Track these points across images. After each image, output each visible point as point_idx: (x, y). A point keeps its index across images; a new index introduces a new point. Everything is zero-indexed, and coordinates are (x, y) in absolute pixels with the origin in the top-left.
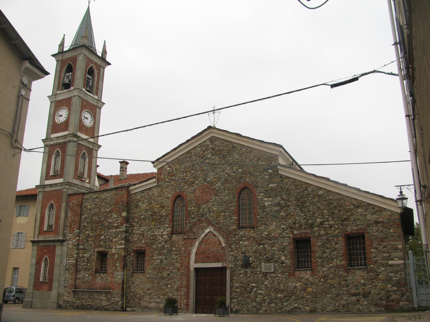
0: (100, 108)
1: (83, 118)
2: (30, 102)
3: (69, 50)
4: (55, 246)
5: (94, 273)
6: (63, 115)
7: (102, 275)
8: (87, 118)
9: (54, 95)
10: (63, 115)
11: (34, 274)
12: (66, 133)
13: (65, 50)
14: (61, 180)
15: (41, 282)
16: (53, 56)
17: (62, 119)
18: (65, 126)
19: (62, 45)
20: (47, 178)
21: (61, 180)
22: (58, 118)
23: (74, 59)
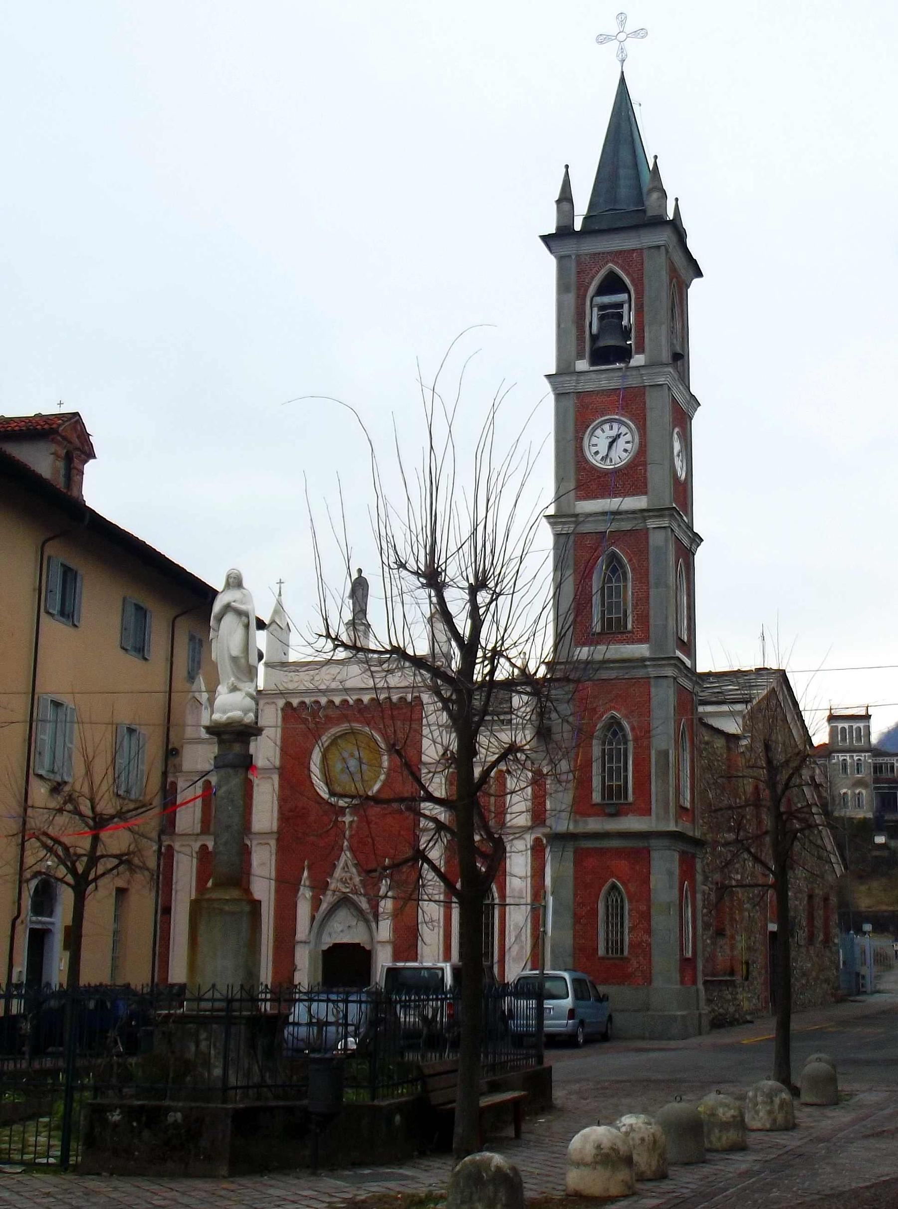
14: (642, 650)
15: (603, 958)
18: (630, 478)
19: (565, 198)
20: (592, 640)
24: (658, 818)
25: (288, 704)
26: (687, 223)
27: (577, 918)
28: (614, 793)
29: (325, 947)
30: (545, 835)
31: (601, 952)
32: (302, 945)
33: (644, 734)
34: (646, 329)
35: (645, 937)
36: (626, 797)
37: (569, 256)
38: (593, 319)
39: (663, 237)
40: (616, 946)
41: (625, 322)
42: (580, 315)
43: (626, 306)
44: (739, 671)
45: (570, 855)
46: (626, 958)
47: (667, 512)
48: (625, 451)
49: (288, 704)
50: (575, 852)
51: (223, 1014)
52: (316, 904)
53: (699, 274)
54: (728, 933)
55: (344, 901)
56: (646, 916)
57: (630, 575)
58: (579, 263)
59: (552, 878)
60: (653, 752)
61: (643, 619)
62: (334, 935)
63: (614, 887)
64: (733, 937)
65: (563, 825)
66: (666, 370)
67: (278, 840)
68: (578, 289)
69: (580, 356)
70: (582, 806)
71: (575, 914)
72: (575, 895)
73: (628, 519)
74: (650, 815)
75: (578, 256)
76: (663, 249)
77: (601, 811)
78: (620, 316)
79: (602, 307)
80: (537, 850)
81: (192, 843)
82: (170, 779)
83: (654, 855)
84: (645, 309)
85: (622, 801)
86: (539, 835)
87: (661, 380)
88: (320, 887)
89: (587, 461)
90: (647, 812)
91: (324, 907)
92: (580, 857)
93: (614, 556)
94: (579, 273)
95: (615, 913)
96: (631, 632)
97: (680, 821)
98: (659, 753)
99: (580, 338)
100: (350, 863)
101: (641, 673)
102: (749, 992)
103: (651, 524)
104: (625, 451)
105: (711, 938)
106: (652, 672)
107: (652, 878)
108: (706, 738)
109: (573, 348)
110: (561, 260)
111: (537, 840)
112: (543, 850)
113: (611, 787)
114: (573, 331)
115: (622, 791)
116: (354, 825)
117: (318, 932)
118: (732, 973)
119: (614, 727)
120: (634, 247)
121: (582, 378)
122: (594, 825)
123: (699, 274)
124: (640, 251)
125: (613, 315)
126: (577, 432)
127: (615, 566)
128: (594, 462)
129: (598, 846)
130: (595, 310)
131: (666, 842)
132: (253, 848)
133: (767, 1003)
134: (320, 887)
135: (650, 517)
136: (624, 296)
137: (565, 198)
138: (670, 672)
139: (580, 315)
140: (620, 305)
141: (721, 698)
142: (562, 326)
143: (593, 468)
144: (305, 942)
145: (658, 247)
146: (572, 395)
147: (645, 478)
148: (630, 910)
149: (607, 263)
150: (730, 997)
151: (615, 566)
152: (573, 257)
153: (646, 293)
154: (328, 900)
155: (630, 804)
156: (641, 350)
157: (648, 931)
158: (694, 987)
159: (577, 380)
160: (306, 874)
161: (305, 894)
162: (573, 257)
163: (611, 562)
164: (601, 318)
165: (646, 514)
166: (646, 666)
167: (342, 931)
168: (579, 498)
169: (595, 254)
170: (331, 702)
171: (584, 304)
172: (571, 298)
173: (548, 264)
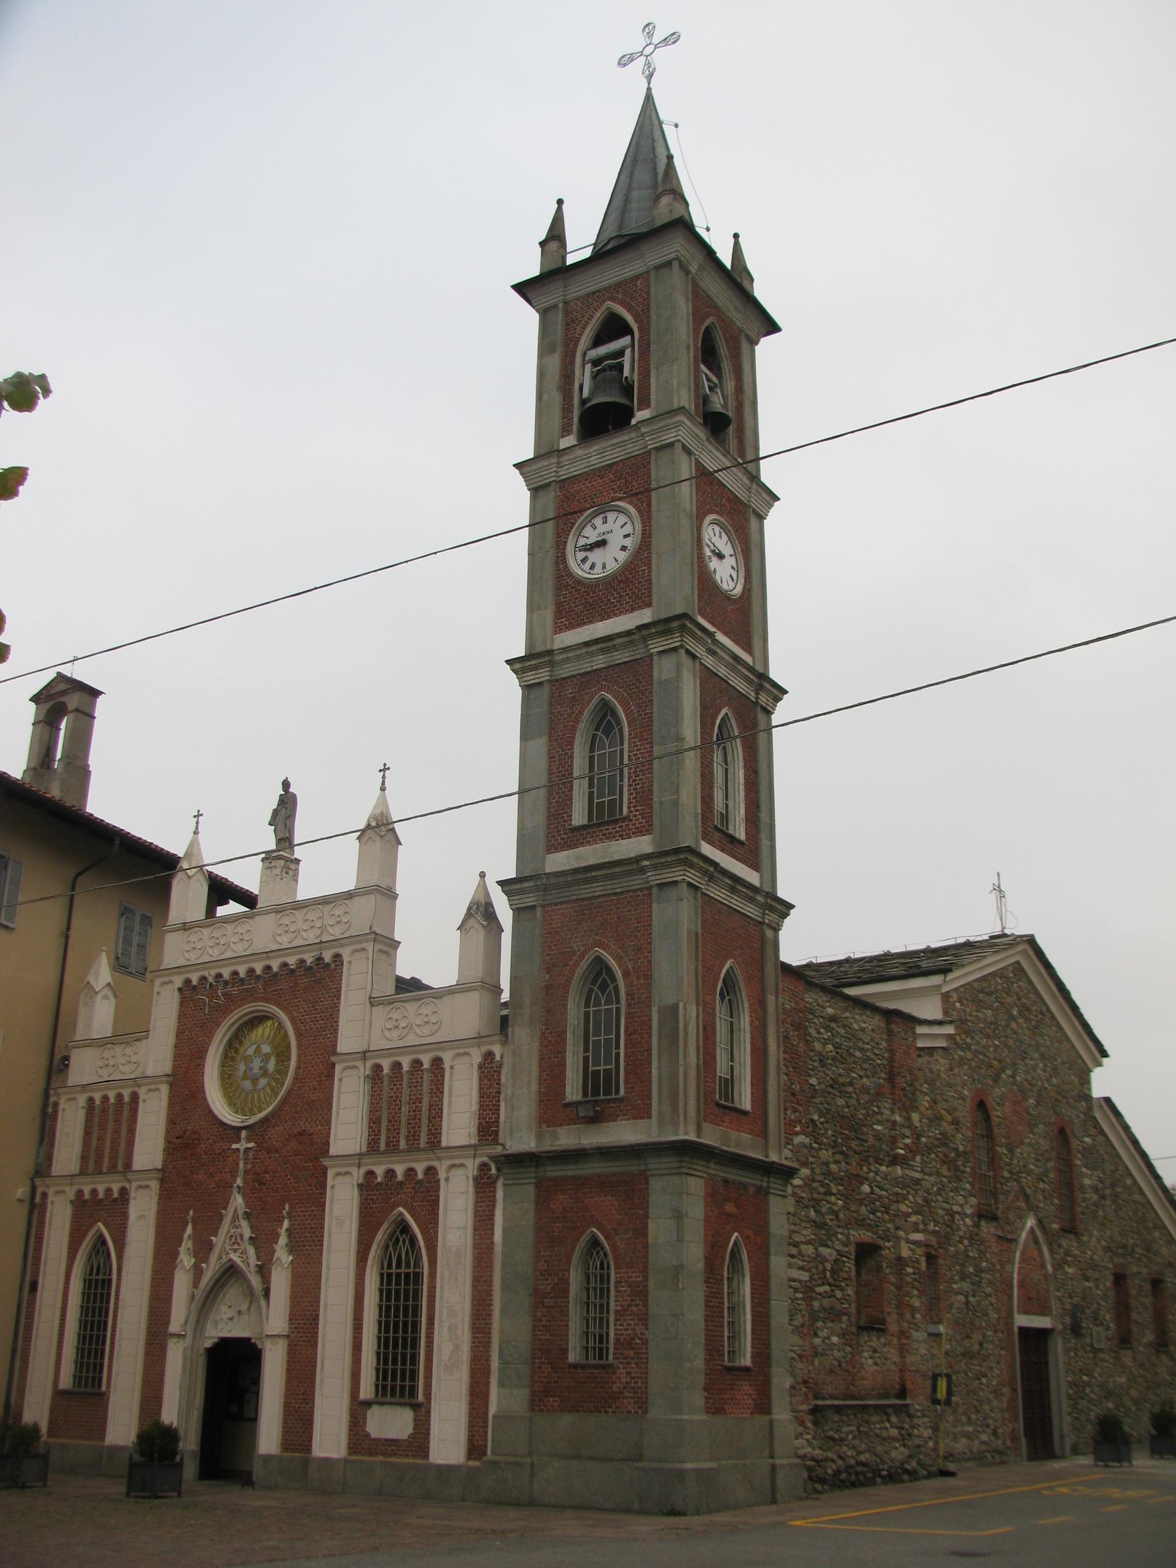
0: (761, 518)
1: (708, 553)
2: (97, 723)
3: (602, 254)
4: (644, 1177)
5: (854, 1329)
6: (608, 542)
7: (874, 1342)
8: (720, 556)
9: (545, 451)
10: (608, 542)
11: (703, 1324)
12: (645, 616)
13: (571, 260)
14: (642, 845)
15: (575, 1366)
16: (522, 288)
17: (610, 560)
18: (631, 584)
19: (556, 235)
20: (572, 837)
21: (642, 845)
22: (581, 555)
23: (635, 291)
24: (661, 1123)
25: (188, 982)
26: (752, 264)
27: (538, 1298)
28: (598, 1084)
29: (208, 1344)
30: (493, 1158)
31: (573, 1357)
32: (175, 1340)
33: (643, 975)
34: (653, 373)
35: (640, 1329)
36: (617, 1092)
37: (555, 306)
38: (585, 378)
39: (675, 246)
40: (597, 1344)
41: (626, 373)
42: (567, 376)
43: (628, 352)
44: (968, 944)
45: (529, 1191)
46: (611, 1366)
47: (675, 624)
48: (624, 548)
49: (188, 982)
50: (538, 1185)
51: (269, 1436)
52: (198, 1272)
53: (772, 327)
54: (893, 1327)
55: (230, 1272)
56: (640, 1293)
57: (626, 730)
58: (567, 312)
59: (504, 1229)
60: (654, 1010)
61: (644, 797)
62: (220, 1326)
63: (595, 1243)
64: (903, 1334)
65: (521, 1138)
66: (676, 419)
67: (162, 1180)
68: (566, 345)
69: (565, 431)
70: (552, 1108)
71: (536, 1290)
72: (537, 1257)
73: (624, 646)
74: (650, 1117)
75: (566, 303)
76: (676, 264)
77: (571, 1114)
78: (620, 367)
79: (596, 362)
80: (484, 1185)
81: (67, 1189)
82: (53, 1099)
83: (656, 1184)
84: (653, 347)
85: (613, 1096)
86: (486, 1159)
87: (669, 437)
88: (203, 1249)
89: (570, 574)
90: (643, 1113)
91: (206, 1279)
92: (545, 1191)
93: (605, 709)
94: (568, 325)
95: (597, 1285)
96: (627, 818)
97: (707, 1127)
98: (662, 1011)
99: (567, 410)
100: (240, 1213)
101: (636, 882)
102: (969, 1421)
103: (656, 646)
104: (624, 548)
105: (843, 1335)
106: (654, 878)
107: (651, 1224)
108: (830, 1011)
109: (556, 422)
110: (544, 314)
111: (484, 1167)
112: (493, 1183)
113: (596, 1073)
114: (557, 398)
115: (610, 1079)
116: (251, 1155)
117: (198, 1321)
118: (902, 1393)
119: (600, 974)
120: (637, 272)
121: (565, 458)
122: (567, 1138)
123: (772, 327)
124: (645, 276)
125: (611, 367)
126: (558, 535)
127: (605, 720)
128: (580, 573)
129: (571, 1173)
130: (588, 367)
131: (667, 1162)
132: (132, 1195)
133: (1014, 1439)
134: (203, 1249)
135: (651, 636)
136: (626, 340)
137: (556, 235)
138: (693, 876)
139: (567, 376)
140: (620, 353)
141: (916, 971)
142: (545, 398)
143: (579, 582)
144: (179, 1336)
145: (669, 264)
146: (553, 485)
147: (650, 581)
148: (618, 1282)
149: (603, 301)
150: (894, 1432)
151: (605, 720)
152: (560, 305)
153: (653, 327)
154: (211, 1269)
155: (621, 1100)
156: (645, 403)
157: (644, 1318)
158: (761, 1419)
159: (558, 463)
160: (189, 1230)
161: (186, 1260)
162: (560, 305)
163: (605, 716)
164: (594, 377)
165: (645, 632)
166: (643, 870)
167: (231, 1319)
168: (558, 629)
169: (588, 295)
170: (251, 971)
171: (572, 363)
172: (555, 361)
173: (527, 319)
